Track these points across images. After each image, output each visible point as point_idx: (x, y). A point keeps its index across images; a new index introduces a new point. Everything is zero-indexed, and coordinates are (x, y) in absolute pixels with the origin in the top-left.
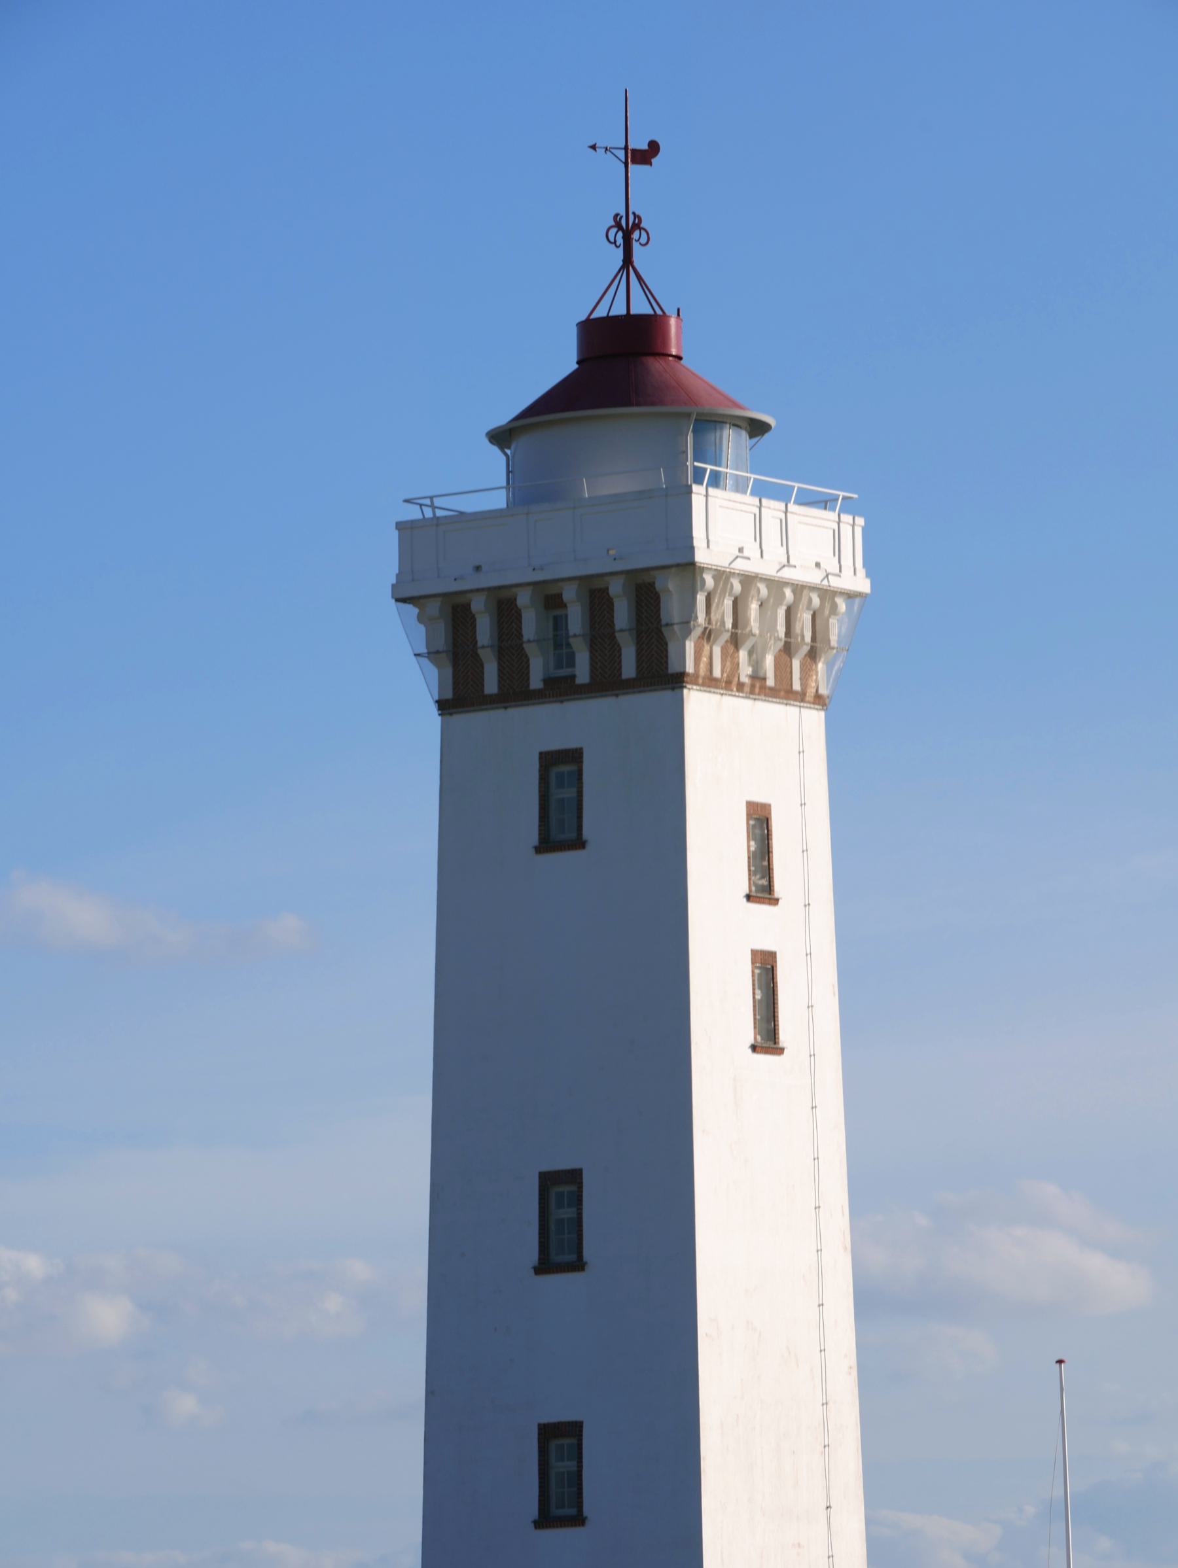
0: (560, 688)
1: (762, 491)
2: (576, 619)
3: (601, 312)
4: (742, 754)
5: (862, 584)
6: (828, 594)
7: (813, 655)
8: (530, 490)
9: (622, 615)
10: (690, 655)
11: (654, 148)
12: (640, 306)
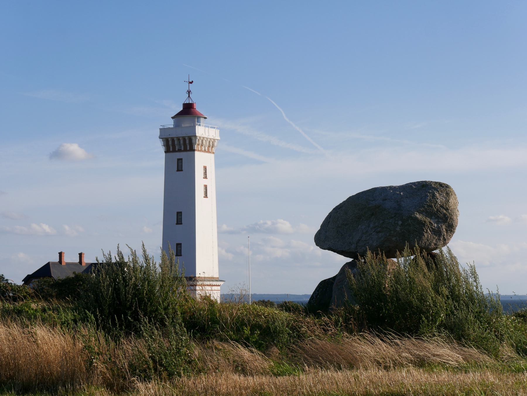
0: (180, 150)
1: (205, 126)
2: (182, 142)
4: (202, 159)
5: (219, 138)
6: (214, 140)
7: (212, 147)
8: (177, 125)
9: (187, 142)
10: (196, 147)
11: (192, 82)
12: (191, 102)
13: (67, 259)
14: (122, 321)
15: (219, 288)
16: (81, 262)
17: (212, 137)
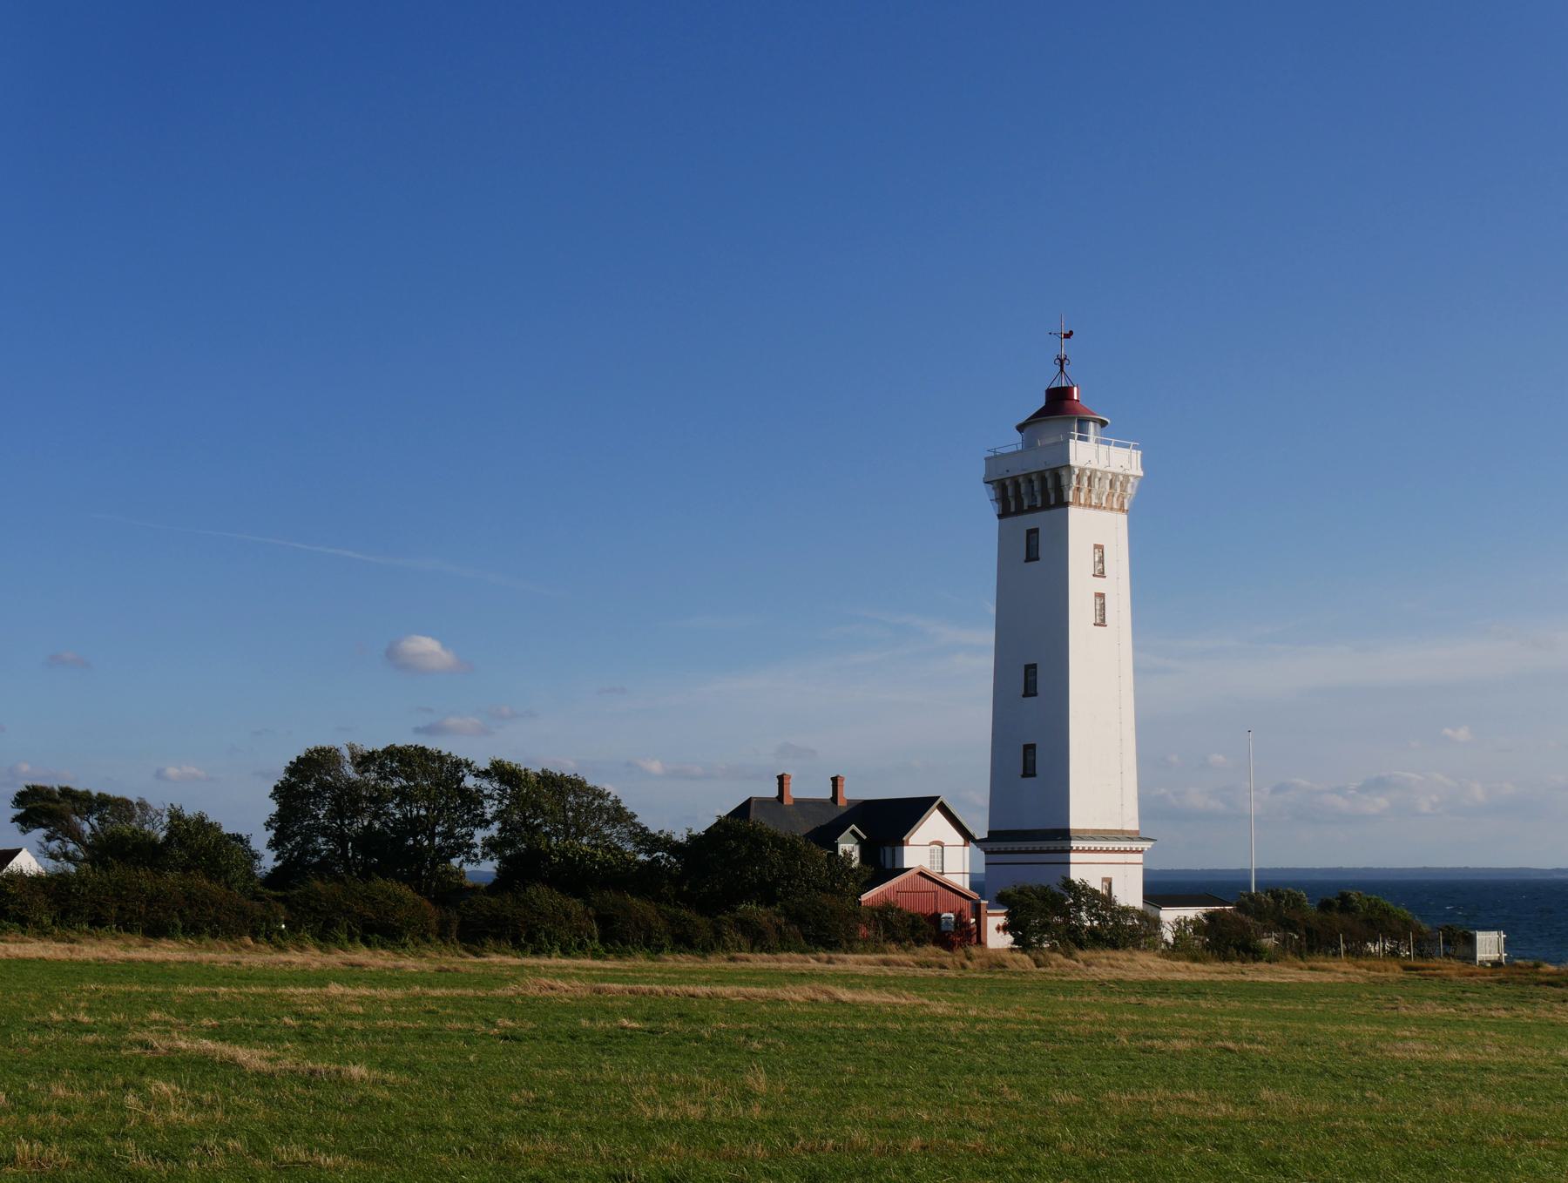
0: (1033, 509)
3: (1054, 385)
5: (1141, 473)
6: (1126, 477)
8: (1029, 445)
13: (795, 791)
14: (104, 1014)
15: (1139, 858)
16: (834, 799)
17: (1120, 471)
